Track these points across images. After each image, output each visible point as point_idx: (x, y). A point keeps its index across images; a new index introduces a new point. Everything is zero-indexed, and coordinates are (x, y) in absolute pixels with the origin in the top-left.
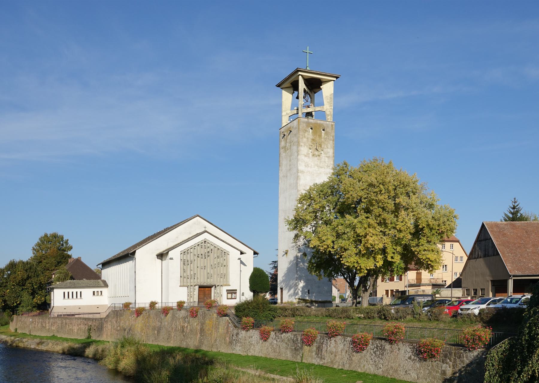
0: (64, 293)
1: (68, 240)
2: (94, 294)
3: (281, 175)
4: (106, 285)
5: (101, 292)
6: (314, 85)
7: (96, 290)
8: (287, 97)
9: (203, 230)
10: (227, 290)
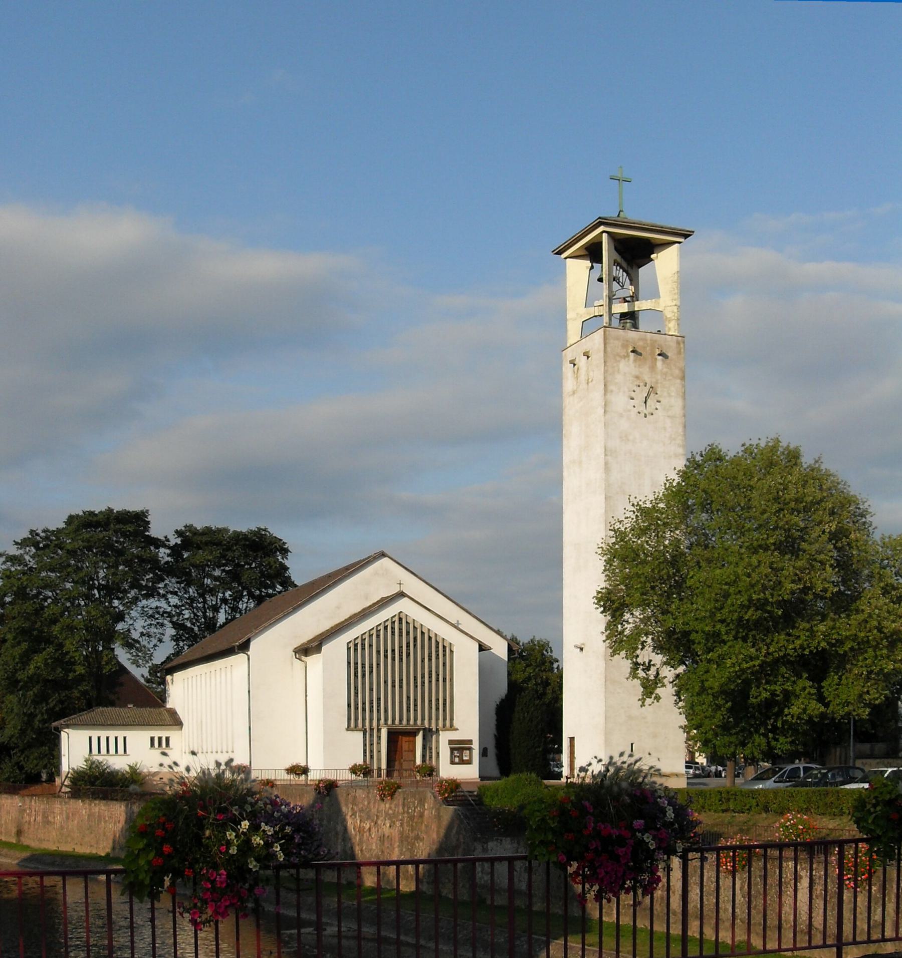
0: (90, 738)
1: (16, 543)
2: (152, 745)
3: (567, 458)
4: (176, 722)
5: (167, 739)
6: (635, 252)
7: (156, 734)
8: (578, 271)
9: (396, 590)
10: (451, 742)
